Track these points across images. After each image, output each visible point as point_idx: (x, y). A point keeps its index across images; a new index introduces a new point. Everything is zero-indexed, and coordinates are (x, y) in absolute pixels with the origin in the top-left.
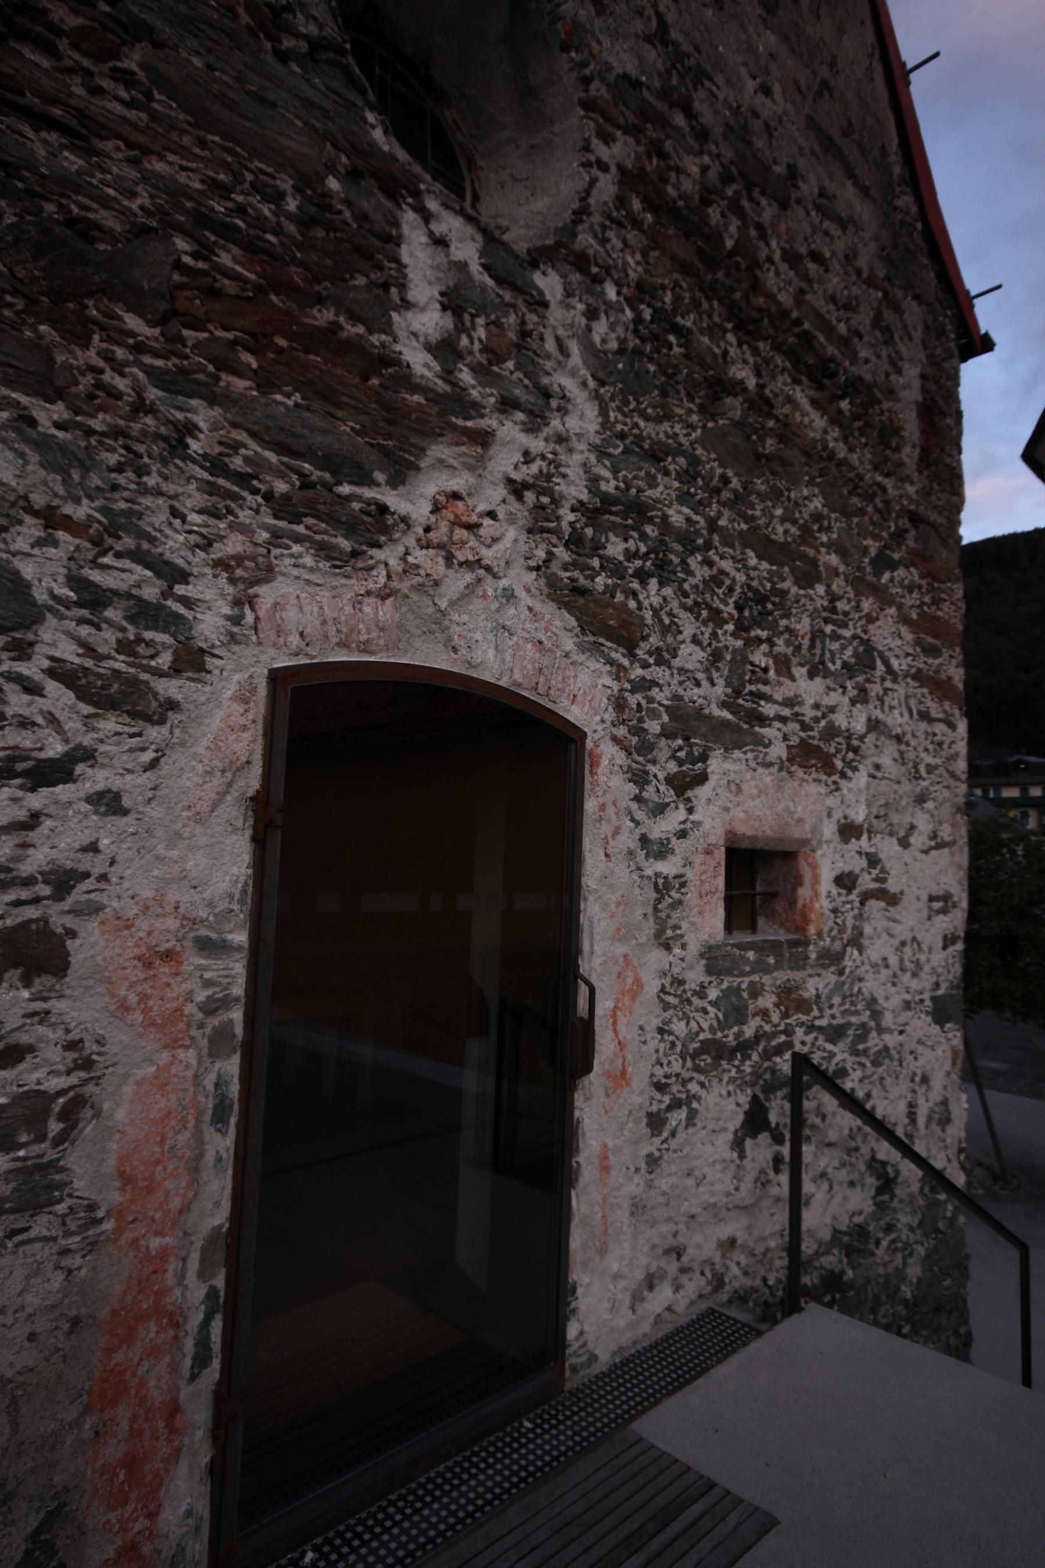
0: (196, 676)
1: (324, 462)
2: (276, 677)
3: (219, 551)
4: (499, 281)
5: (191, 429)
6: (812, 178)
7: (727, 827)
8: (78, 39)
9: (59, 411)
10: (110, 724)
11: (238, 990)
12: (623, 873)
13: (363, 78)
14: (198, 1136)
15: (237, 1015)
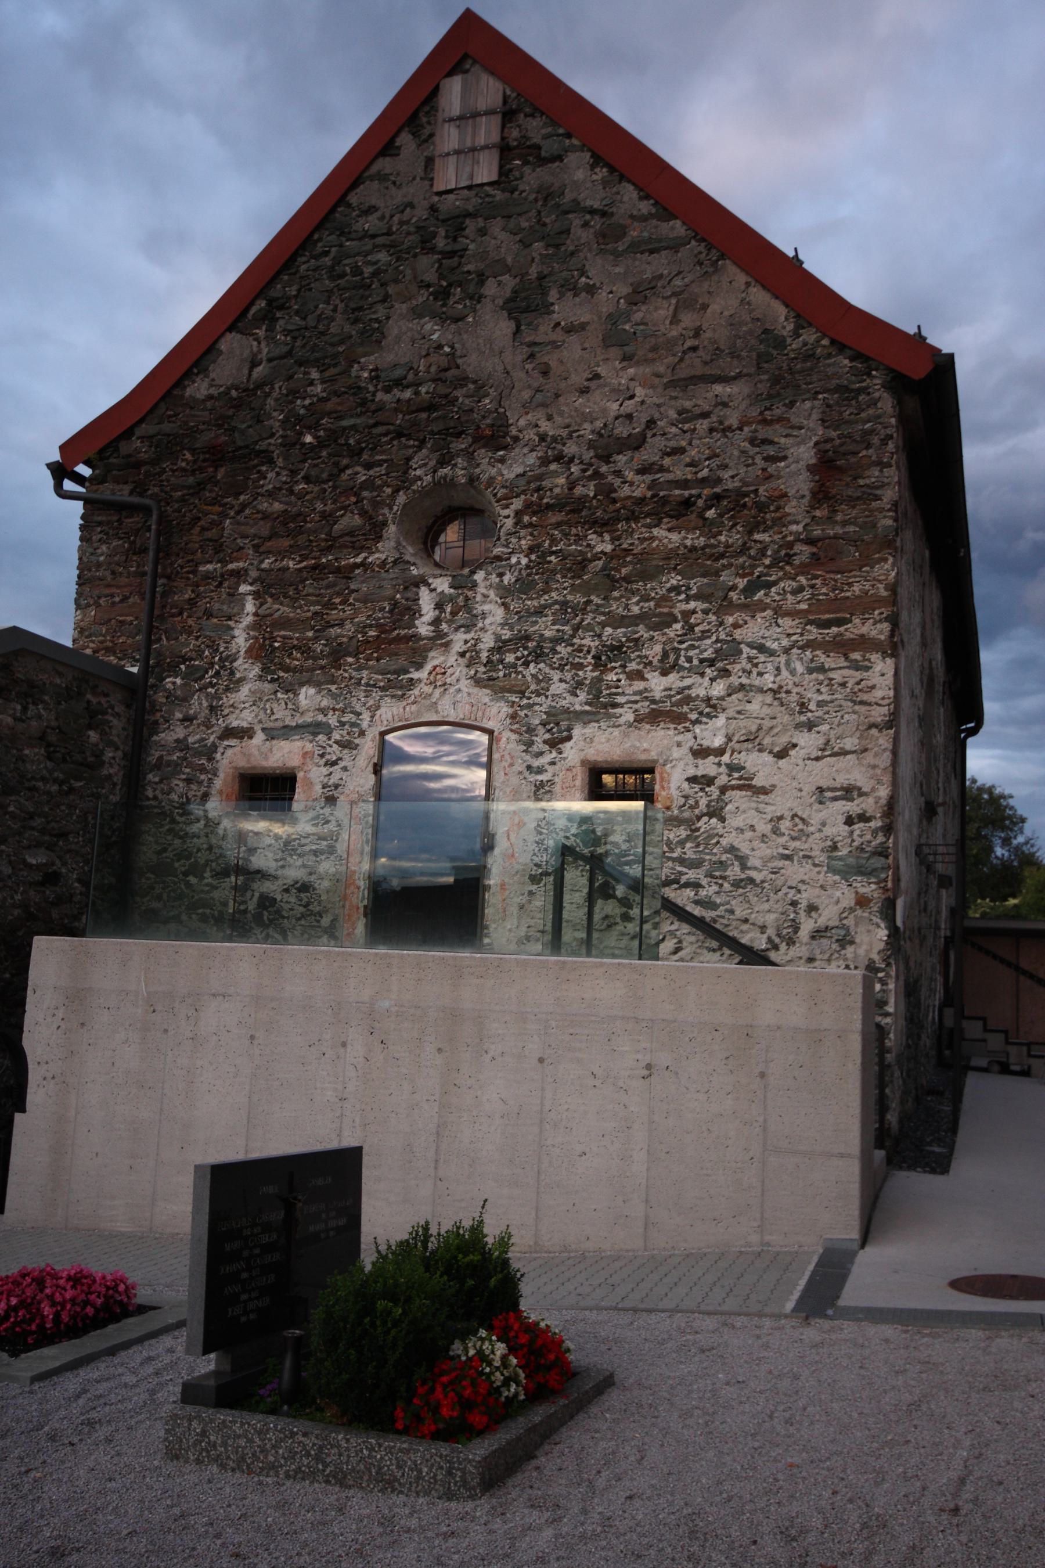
0: (939, 688)
1: (395, 672)
3: (368, 705)
8: (341, 603)
9: (335, 686)
10: (346, 751)
11: (371, 812)
14: (362, 846)
15: (371, 818)
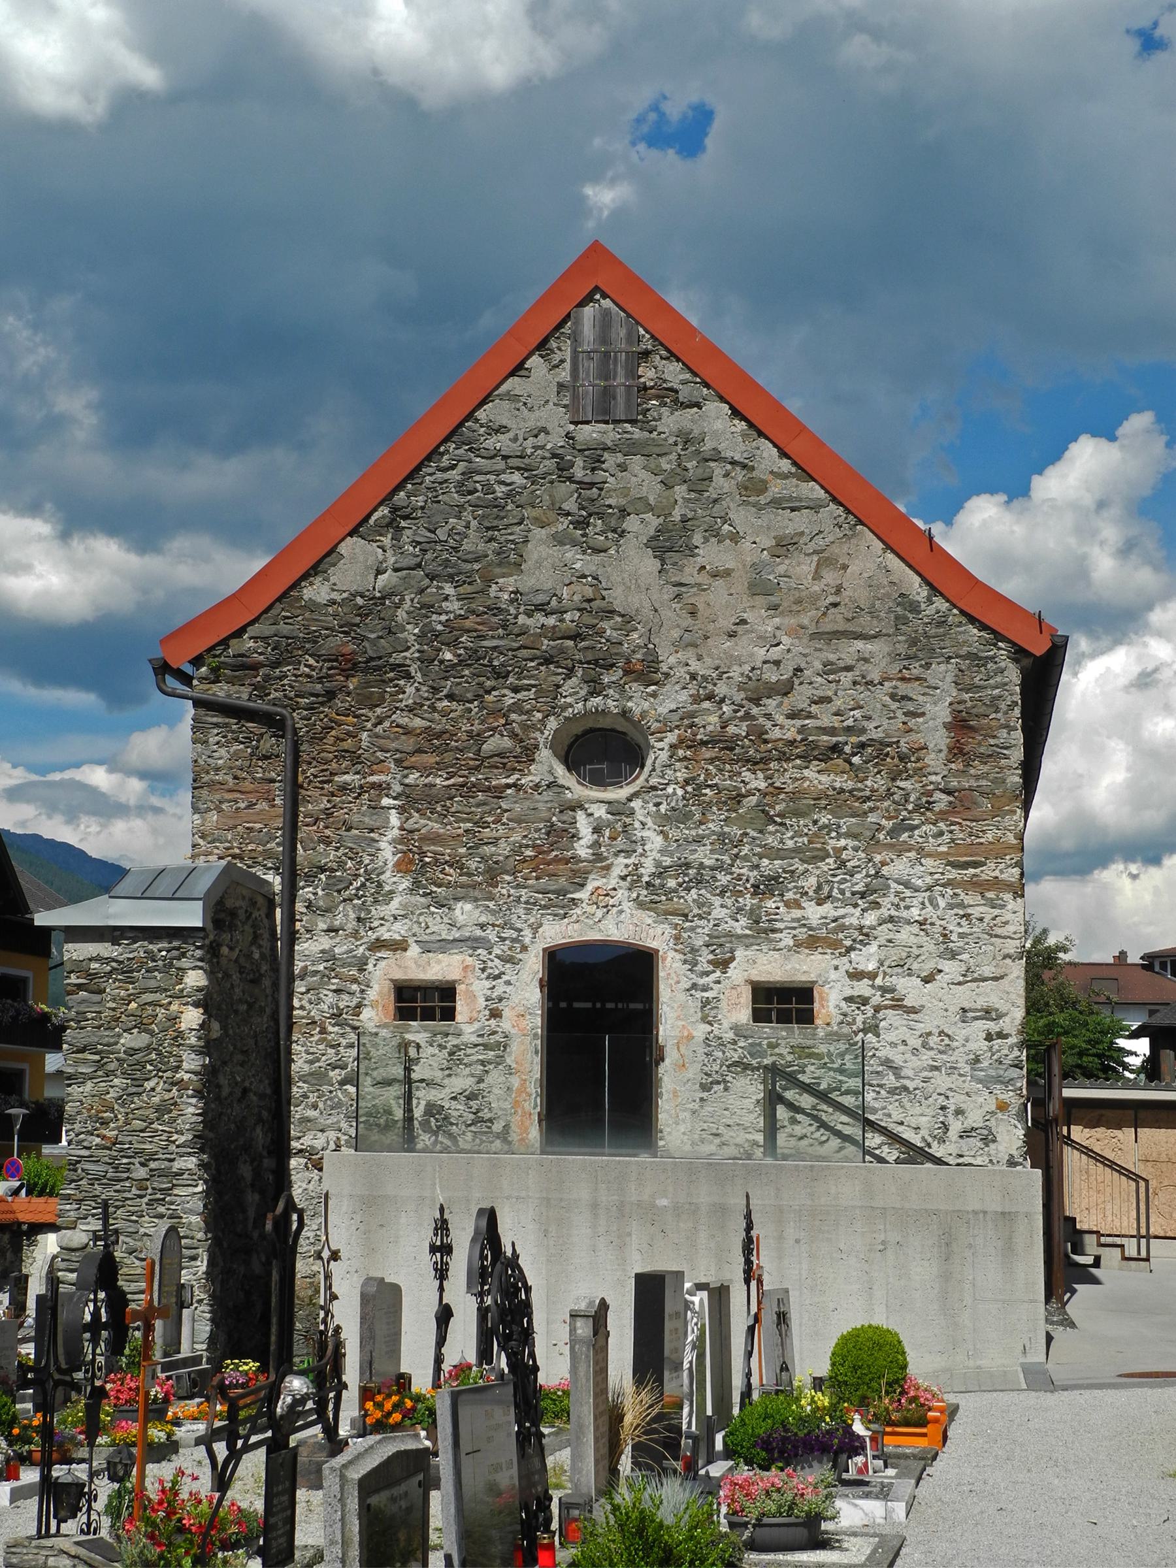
2: (544, 950)
4: (613, 814)
5: (521, 896)
6: (723, 878)
7: (1145, 54)
10: (508, 966)
12: (682, 997)
13: (93, 1555)
15: (539, 1031)
